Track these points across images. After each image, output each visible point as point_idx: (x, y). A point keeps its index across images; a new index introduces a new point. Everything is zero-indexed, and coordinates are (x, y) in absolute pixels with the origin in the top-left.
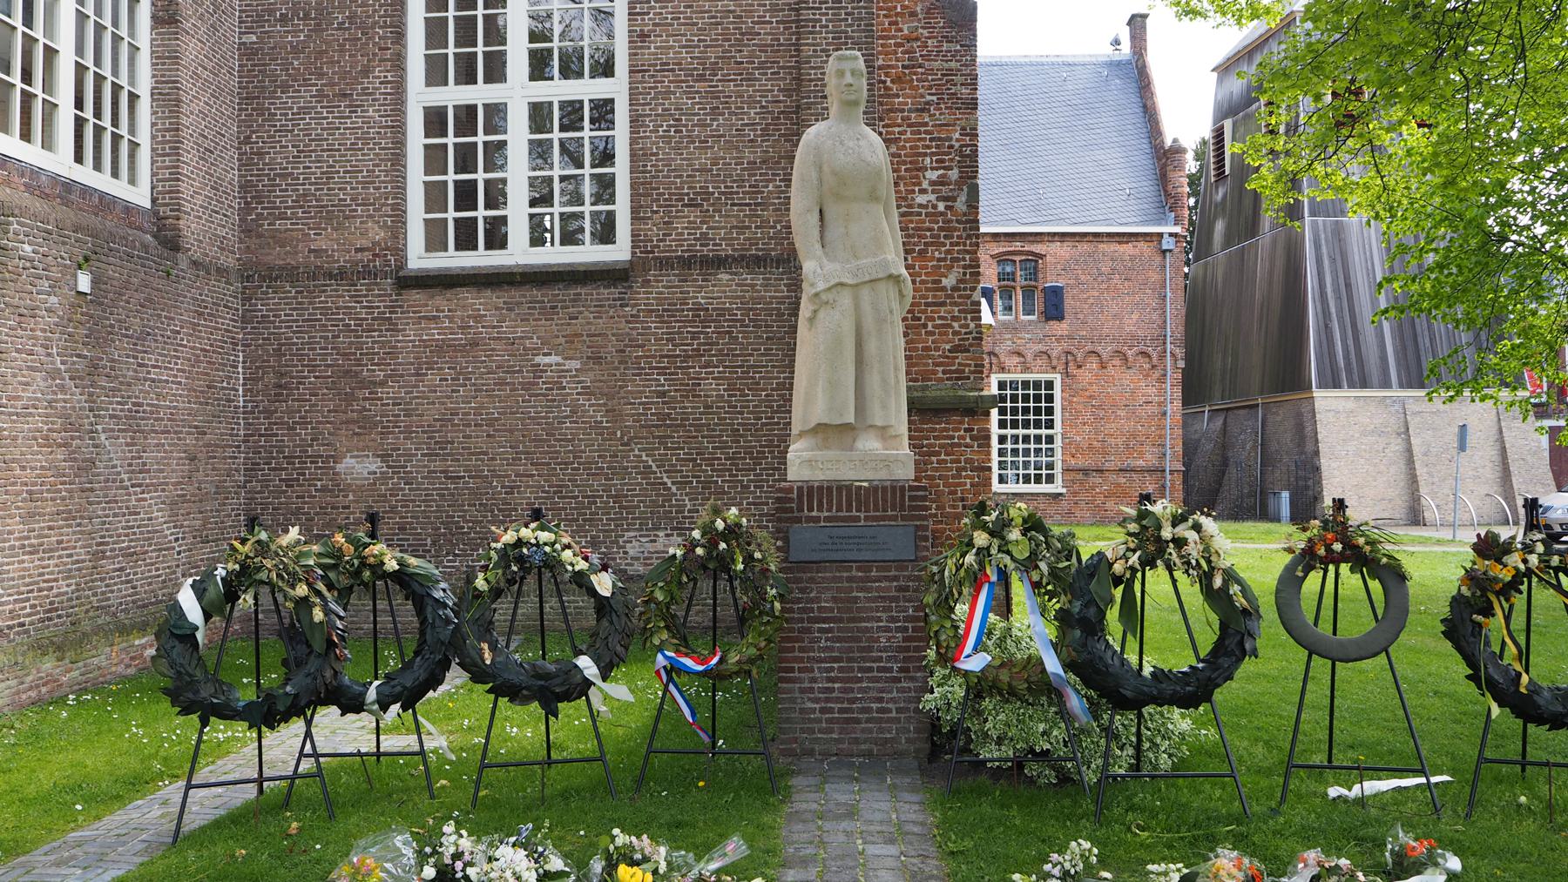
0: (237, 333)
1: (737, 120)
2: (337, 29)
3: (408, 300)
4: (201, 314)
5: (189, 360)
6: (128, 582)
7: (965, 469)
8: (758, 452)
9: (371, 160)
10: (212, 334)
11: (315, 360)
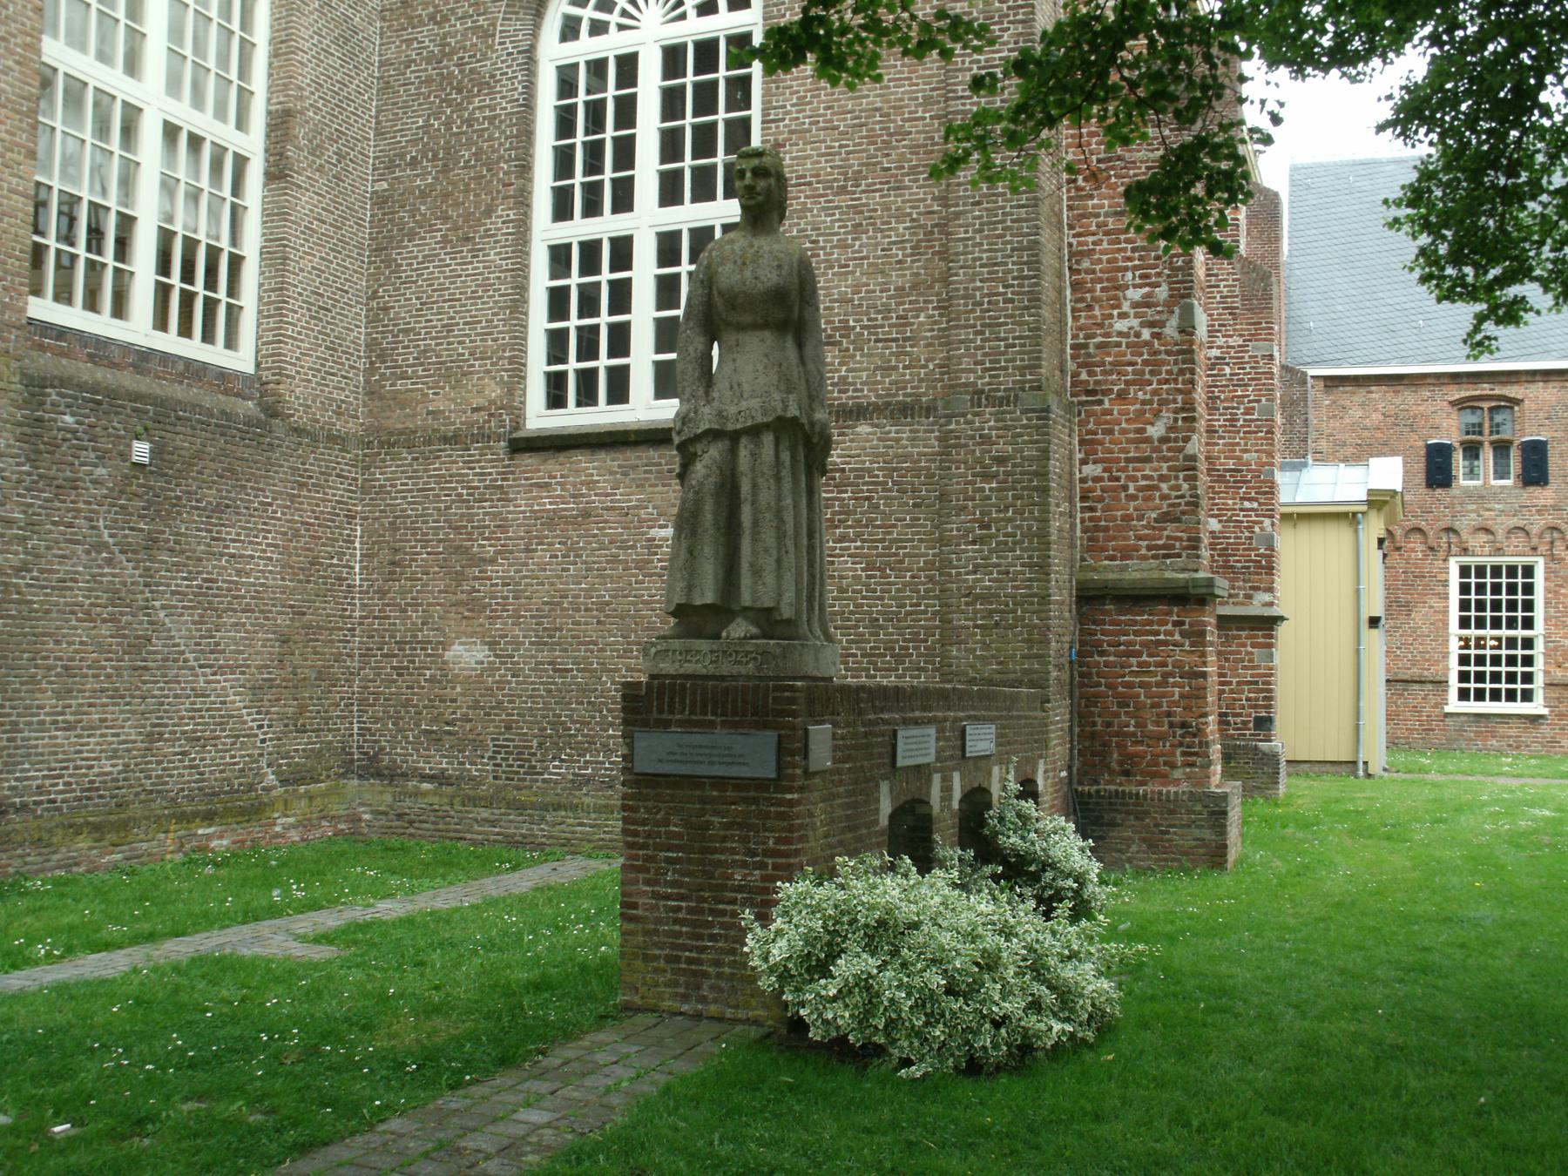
0: (355, 505)
1: (884, 237)
2: (463, 168)
3: (520, 466)
4: (302, 485)
5: (285, 534)
6: (192, 767)
7: (1172, 674)
8: (901, 648)
9: (490, 309)
10: (318, 505)
11: (427, 534)
